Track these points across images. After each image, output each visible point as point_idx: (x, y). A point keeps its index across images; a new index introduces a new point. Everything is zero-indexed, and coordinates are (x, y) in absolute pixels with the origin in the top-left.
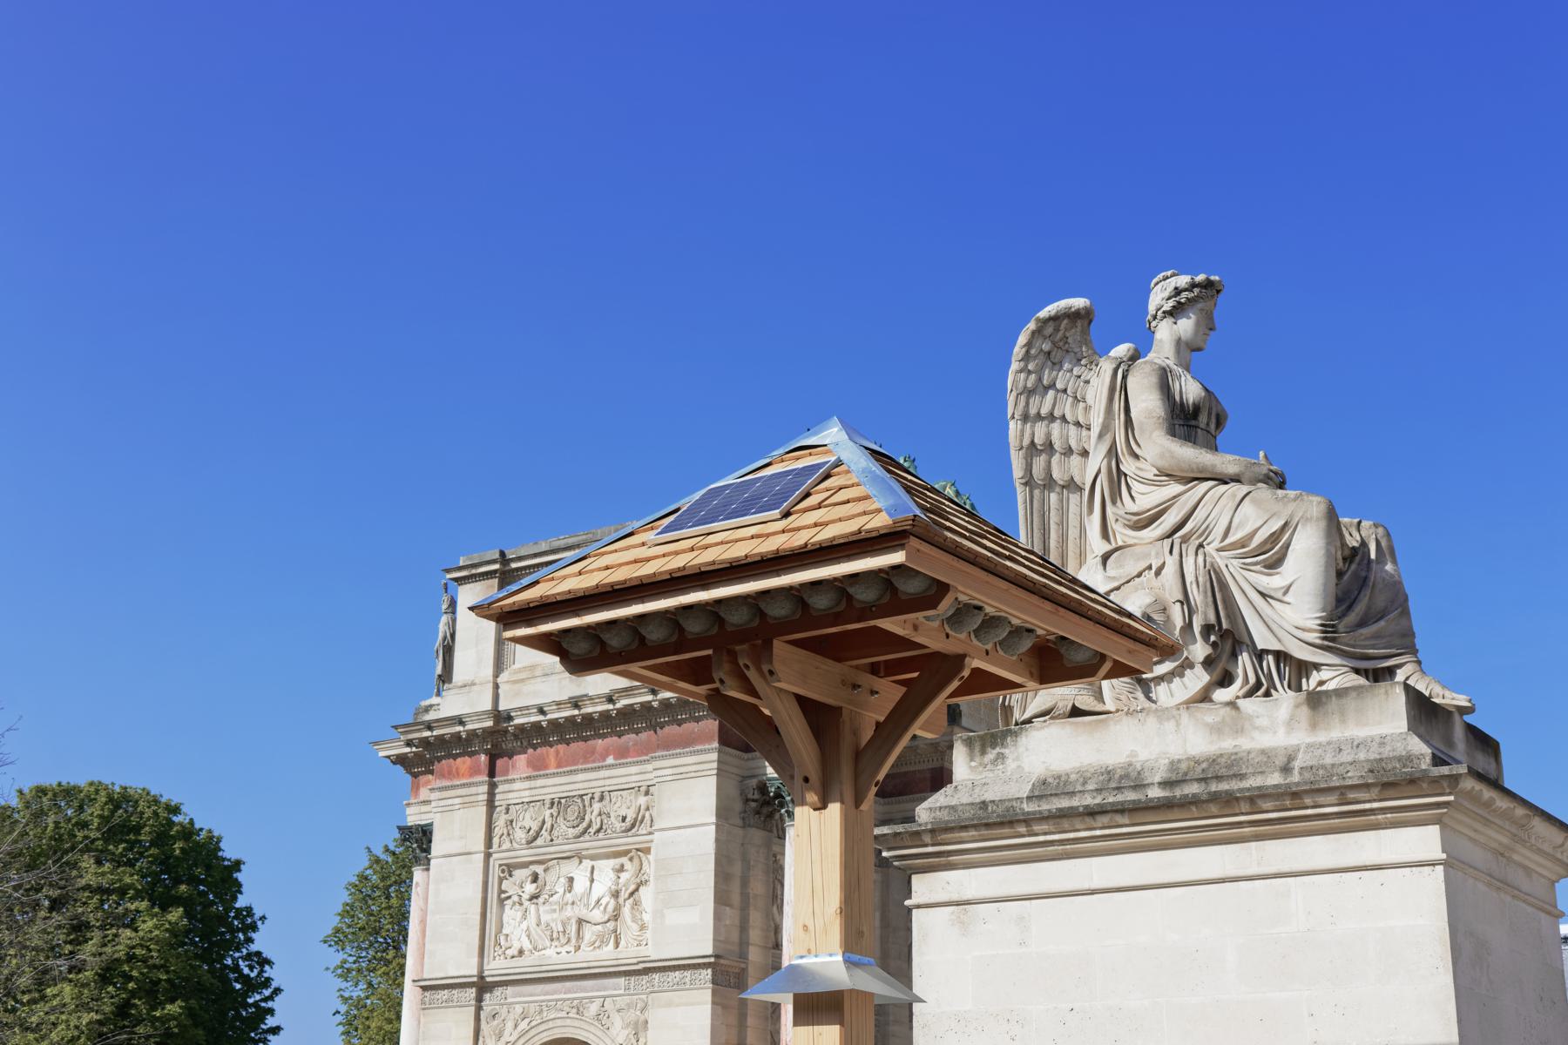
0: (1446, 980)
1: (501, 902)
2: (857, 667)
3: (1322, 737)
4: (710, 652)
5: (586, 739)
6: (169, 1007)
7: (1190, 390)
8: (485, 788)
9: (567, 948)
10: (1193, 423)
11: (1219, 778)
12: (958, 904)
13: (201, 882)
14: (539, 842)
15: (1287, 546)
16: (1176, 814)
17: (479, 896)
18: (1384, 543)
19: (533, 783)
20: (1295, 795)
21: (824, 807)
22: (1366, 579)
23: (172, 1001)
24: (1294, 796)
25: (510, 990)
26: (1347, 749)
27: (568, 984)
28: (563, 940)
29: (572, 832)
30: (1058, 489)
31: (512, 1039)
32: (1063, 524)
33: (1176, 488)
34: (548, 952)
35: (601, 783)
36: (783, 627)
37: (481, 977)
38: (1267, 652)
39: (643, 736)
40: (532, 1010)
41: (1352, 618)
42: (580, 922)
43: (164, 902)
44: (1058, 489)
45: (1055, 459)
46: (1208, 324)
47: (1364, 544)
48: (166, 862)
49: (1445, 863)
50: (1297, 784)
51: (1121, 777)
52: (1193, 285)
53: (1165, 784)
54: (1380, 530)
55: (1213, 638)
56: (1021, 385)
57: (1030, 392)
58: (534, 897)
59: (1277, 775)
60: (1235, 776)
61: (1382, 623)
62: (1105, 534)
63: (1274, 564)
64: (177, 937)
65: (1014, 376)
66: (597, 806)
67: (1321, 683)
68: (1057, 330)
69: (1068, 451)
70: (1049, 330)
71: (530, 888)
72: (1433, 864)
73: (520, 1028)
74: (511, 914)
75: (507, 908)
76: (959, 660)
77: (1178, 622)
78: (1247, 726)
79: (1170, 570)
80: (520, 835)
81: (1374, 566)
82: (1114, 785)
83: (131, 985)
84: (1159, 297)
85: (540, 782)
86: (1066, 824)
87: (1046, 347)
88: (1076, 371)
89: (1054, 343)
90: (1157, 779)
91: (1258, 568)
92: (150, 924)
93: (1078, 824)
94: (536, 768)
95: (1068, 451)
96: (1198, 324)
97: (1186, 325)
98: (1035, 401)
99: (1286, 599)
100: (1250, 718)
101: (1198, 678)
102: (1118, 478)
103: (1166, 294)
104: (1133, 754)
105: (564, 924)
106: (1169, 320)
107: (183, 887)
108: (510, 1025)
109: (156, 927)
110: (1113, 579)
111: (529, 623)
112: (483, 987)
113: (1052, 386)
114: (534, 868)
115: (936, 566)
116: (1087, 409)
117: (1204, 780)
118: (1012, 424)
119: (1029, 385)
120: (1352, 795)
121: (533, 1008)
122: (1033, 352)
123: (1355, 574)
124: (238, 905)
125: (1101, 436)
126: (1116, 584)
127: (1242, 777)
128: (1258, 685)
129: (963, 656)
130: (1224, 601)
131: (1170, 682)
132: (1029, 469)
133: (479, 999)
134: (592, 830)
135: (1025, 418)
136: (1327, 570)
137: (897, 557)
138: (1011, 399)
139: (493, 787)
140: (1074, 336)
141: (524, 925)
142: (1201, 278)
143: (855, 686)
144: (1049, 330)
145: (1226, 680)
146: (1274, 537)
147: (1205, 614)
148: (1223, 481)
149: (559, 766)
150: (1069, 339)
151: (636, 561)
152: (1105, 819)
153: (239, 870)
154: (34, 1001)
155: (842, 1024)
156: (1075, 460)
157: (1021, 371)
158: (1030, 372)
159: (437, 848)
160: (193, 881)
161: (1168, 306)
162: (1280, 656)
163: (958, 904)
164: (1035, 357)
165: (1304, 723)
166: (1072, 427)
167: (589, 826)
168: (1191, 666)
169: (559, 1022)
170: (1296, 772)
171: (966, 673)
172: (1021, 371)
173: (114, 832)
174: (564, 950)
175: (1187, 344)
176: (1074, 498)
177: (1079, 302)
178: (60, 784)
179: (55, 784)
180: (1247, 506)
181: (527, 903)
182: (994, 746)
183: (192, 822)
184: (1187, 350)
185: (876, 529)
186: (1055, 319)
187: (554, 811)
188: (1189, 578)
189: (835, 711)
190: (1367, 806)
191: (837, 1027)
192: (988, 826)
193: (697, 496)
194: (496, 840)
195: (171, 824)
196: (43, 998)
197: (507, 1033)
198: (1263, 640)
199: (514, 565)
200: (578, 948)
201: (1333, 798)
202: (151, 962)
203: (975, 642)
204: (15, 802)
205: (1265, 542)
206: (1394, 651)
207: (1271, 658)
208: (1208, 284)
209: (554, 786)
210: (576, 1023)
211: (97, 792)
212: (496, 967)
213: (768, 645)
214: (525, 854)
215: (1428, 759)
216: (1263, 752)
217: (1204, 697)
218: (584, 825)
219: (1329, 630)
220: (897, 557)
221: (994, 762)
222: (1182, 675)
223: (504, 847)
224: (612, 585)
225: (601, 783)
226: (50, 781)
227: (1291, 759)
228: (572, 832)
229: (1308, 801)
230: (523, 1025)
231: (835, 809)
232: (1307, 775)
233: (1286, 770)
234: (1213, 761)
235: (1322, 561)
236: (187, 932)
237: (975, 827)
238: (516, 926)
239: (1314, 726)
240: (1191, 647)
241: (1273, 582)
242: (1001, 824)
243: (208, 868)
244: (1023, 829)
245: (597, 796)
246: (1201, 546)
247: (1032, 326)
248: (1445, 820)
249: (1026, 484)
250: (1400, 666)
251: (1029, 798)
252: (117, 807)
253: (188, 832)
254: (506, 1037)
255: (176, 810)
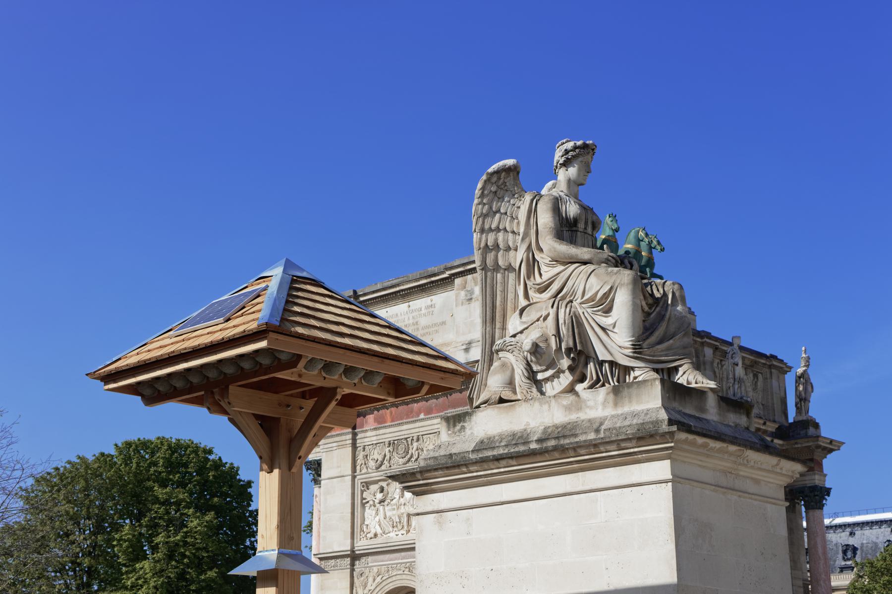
0: (672, 546)
1: (363, 505)
2: (291, 395)
3: (620, 411)
4: (203, 393)
5: (407, 404)
6: (209, 573)
7: (572, 209)
8: (350, 436)
9: (402, 532)
10: (574, 229)
11: (565, 437)
12: (437, 512)
13: (227, 495)
14: (383, 467)
15: (613, 300)
16: (539, 458)
17: (350, 502)
18: (677, 294)
19: (378, 432)
20: (595, 446)
21: (272, 471)
22: (664, 316)
23: (211, 569)
24: (594, 446)
25: (370, 558)
26: (629, 418)
27: (403, 554)
28: (400, 527)
29: (401, 461)
30: (502, 271)
31: (372, 588)
32: (505, 291)
33: (562, 268)
34: (392, 535)
35: (417, 430)
36: (233, 379)
37: (353, 551)
38: (605, 361)
39: (441, 400)
40: (383, 571)
41: (653, 339)
42: (409, 515)
43: (202, 508)
44: (502, 271)
45: (500, 254)
46: (586, 169)
47: (665, 295)
48: (205, 484)
49: (672, 481)
50: (595, 439)
51: (519, 438)
52: (575, 148)
53: (539, 441)
54: (676, 287)
55: (572, 355)
56: (479, 212)
57: (484, 216)
58: (382, 501)
59: (593, 434)
60: (572, 435)
61: (671, 341)
62: (526, 296)
63: (608, 311)
64: (214, 530)
65: (476, 208)
66: (415, 444)
67: (635, 378)
68: (499, 179)
69: (508, 249)
70: (494, 179)
71: (379, 496)
72: (666, 482)
73: (376, 581)
74: (369, 512)
75: (367, 508)
76: (333, 391)
77: (554, 346)
78: (583, 405)
79: (551, 319)
80: (372, 464)
81: (669, 308)
82: (514, 442)
83: (186, 560)
84: (558, 157)
85: (382, 431)
86: (485, 466)
87: (494, 189)
88: (512, 201)
89: (498, 186)
90: (535, 438)
91: (599, 313)
92: (196, 522)
93: (491, 465)
94: (379, 423)
95: (508, 249)
96: (579, 170)
97: (573, 171)
98: (488, 221)
99: (615, 330)
100: (585, 401)
101: (566, 379)
102: (532, 264)
103: (561, 154)
104: (528, 424)
105: (399, 517)
106: (563, 169)
107: (216, 499)
108: (371, 579)
109: (198, 525)
110: (524, 323)
111: (115, 381)
112: (354, 557)
113: (498, 211)
114: (381, 484)
115: (288, 347)
116: (518, 223)
117: (557, 438)
118: (475, 235)
119: (484, 212)
120: (623, 445)
121: (383, 569)
122: (486, 192)
123: (659, 313)
124: (250, 509)
125: (523, 239)
126: (526, 326)
127: (576, 435)
128: (598, 380)
129: (337, 388)
130: (579, 334)
131: (552, 381)
132: (484, 261)
133: (352, 565)
134: (413, 459)
135: (482, 231)
136: (634, 311)
137: (263, 344)
138: (474, 221)
139: (355, 435)
140: (510, 181)
141: (377, 519)
142: (579, 143)
143: (288, 406)
144: (494, 179)
145: (582, 379)
146: (606, 295)
147: (567, 342)
148: (585, 263)
149: (392, 421)
150: (506, 183)
151: (161, 347)
152: (504, 462)
153: (250, 487)
154: (131, 572)
155: (277, 587)
156: (512, 253)
157: (479, 204)
158: (484, 204)
159: (325, 473)
160: (224, 495)
161: (561, 162)
162: (612, 364)
163: (437, 512)
164: (487, 195)
165: (611, 404)
166: (510, 234)
167: (412, 457)
168: (563, 372)
169: (399, 577)
170: (602, 432)
171: (339, 397)
172: (479, 204)
173: (172, 466)
174: (400, 533)
175: (575, 182)
176: (512, 276)
177: (510, 162)
178: (139, 440)
179: (136, 440)
180: (593, 278)
181: (378, 505)
182: (459, 422)
183: (220, 459)
184: (574, 185)
185: (251, 330)
186: (497, 172)
187: (391, 448)
188: (561, 321)
189: (277, 420)
190: (632, 450)
191: (274, 588)
192: (447, 468)
193: (196, 313)
194: (358, 468)
195: (208, 460)
196: (134, 570)
197: (369, 584)
198: (602, 355)
199: (362, 299)
200: (408, 532)
201: (614, 447)
202: (197, 545)
203: (345, 379)
204: (113, 452)
205: (601, 298)
206: (677, 357)
207: (607, 365)
208: (585, 146)
209: (390, 433)
210: (409, 577)
211: (162, 443)
212: (362, 544)
213: (227, 387)
214: (376, 476)
215: (666, 422)
216: (590, 420)
217: (571, 390)
218: (409, 456)
219: (638, 350)
220: (263, 344)
221: (460, 431)
222: (558, 377)
223: (363, 472)
224: (145, 361)
225: (417, 430)
226: (133, 437)
227: (601, 424)
228: (401, 461)
229: (602, 449)
230: (378, 579)
231: (276, 472)
232: (607, 433)
233: (597, 431)
234: (564, 427)
235: (631, 309)
236: (220, 527)
237: (441, 469)
238: (373, 519)
239: (616, 405)
240: (561, 361)
241: (606, 321)
242: (454, 467)
243: (231, 486)
244: (465, 469)
245: (415, 438)
246: (571, 301)
247: (484, 177)
248: (673, 456)
249: (482, 269)
250: (681, 366)
251: (473, 451)
252: (173, 453)
253: (218, 464)
254: (369, 587)
255: (210, 452)
